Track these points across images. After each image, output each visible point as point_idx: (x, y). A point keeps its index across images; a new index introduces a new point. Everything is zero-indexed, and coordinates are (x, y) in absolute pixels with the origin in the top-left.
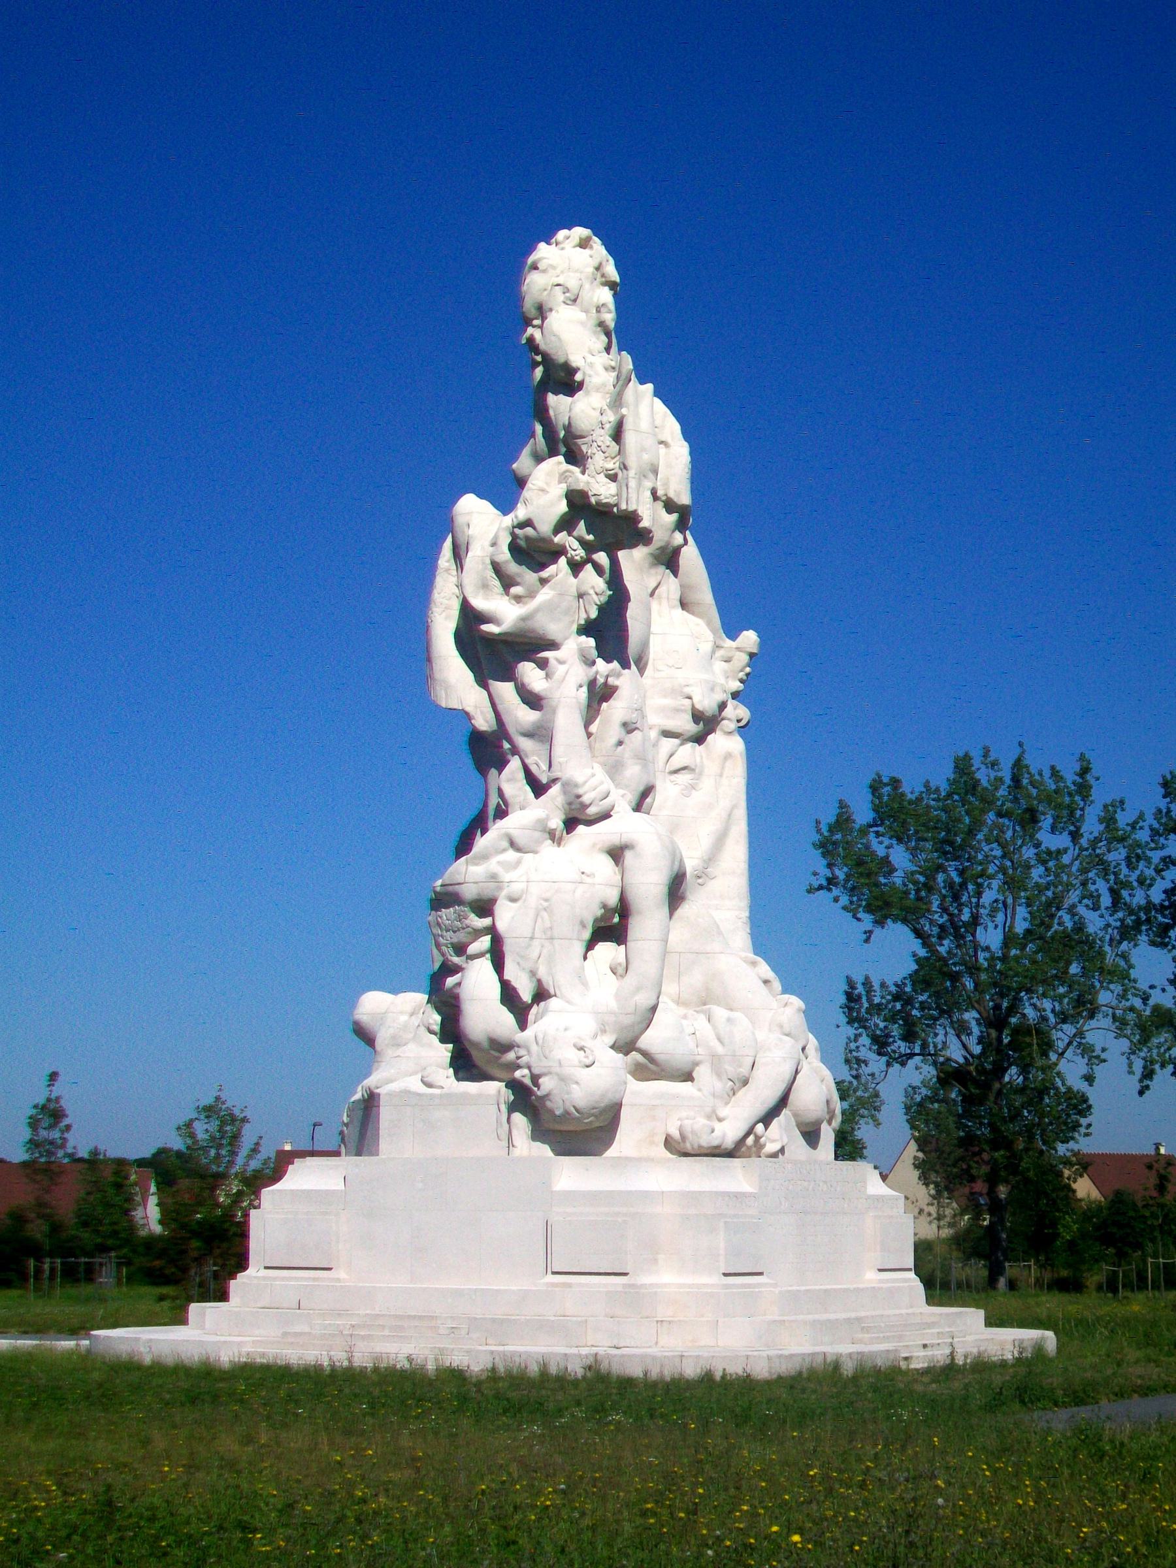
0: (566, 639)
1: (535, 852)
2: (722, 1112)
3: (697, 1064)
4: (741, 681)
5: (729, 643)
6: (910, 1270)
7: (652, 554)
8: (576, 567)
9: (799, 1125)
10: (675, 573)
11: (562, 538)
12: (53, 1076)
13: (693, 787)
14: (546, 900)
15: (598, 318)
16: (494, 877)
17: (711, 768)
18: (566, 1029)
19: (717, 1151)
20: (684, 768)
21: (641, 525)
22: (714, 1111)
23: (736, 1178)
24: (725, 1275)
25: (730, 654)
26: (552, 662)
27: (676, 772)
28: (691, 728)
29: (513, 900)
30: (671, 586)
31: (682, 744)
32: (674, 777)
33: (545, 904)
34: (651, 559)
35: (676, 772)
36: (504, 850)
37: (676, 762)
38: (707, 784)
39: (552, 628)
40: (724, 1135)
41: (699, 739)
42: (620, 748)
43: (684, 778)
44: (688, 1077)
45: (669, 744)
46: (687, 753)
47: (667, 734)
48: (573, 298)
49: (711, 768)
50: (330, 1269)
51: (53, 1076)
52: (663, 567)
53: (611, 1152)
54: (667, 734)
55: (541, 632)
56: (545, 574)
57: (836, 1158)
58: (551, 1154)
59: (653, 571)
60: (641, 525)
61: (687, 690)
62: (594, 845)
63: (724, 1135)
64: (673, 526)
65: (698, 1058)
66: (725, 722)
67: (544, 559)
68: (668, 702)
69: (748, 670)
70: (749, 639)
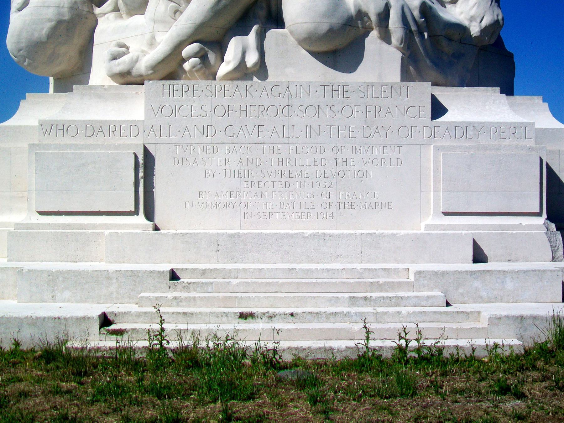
6: (539, 214)
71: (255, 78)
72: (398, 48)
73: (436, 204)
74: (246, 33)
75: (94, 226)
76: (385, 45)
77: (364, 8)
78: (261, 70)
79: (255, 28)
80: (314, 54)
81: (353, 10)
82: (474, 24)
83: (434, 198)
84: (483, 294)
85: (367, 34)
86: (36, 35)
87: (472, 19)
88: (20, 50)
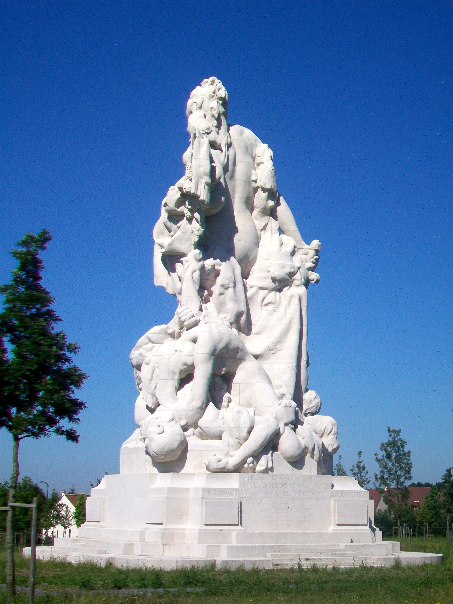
0: (189, 251)
1: (162, 343)
2: (232, 453)
3: (223, 432)
4: (313, 262)
5: (307, 246)
6: (366, 525)
7: (260, 211)
8: (190, 220)
9: (286, 458)
10: (276, 219)
11: (182, 209)
12: (360, 453)
13: (275, 311)
14: (158, 363)
15: (211, 113)
16: (141, 355)
17: (285, 302)
18: (156, 418)
19: (224, 470)
20: (270, 303)
21: (200, 199)
22: (228, 453)
23: (233, 482)
24: (147, 523)
25: (307, 252)
26: (184, 262)
27: (267, 305)
28: (272, 285)
29: (147, 364)
30: (273, 224)
31: (269, 293)
32: (266, 307)
33: (157, 365)
34: (261, 214)
35: (267, 305)
36: (147, 343)
37: (266, 301)
38: (282, 309)
39: (182, 248)
40: (227, 463)
41: (280, 290)
42: (222, 296)
43: (270, 307)
44: (220, 438)
45: (263, 293)
46: (271, 296)
47: (262, 289)
48: (199, 107)
49: (285, 302)
50: (99, 522)
51: (360, 453)
52: (269, 217)
53: (183, 471)
54: (262, 289)
55: (177, 250)
56: (178, 225)
57: (318, 474)
58: (157, 472)
59: (263, 219)
60: (200, 199)
61: (269, 269)
62: (186, 338)
63: (227, 463)
64: (266, 198)
65: (223, 429)
66: (295, 281)
67: (177, 219)
68: (262, 274)
69: (316, 257)
70: (315, 243)
71: (270, 472)
72: (316, 461)
73: (334, 521)
74: (267, 454)
75: (231, 530)
76: (312, 459)
77: (307, 446)
78: (272, 469)
79: (271, 452)
80: (289, 462)
81: (304, 446)
82: (330, 447)
83: (333, 519)
84: (364, 553)
85: (306, 455)
86: (173, 447)
87: (329, 445)
88: (162, 452)
